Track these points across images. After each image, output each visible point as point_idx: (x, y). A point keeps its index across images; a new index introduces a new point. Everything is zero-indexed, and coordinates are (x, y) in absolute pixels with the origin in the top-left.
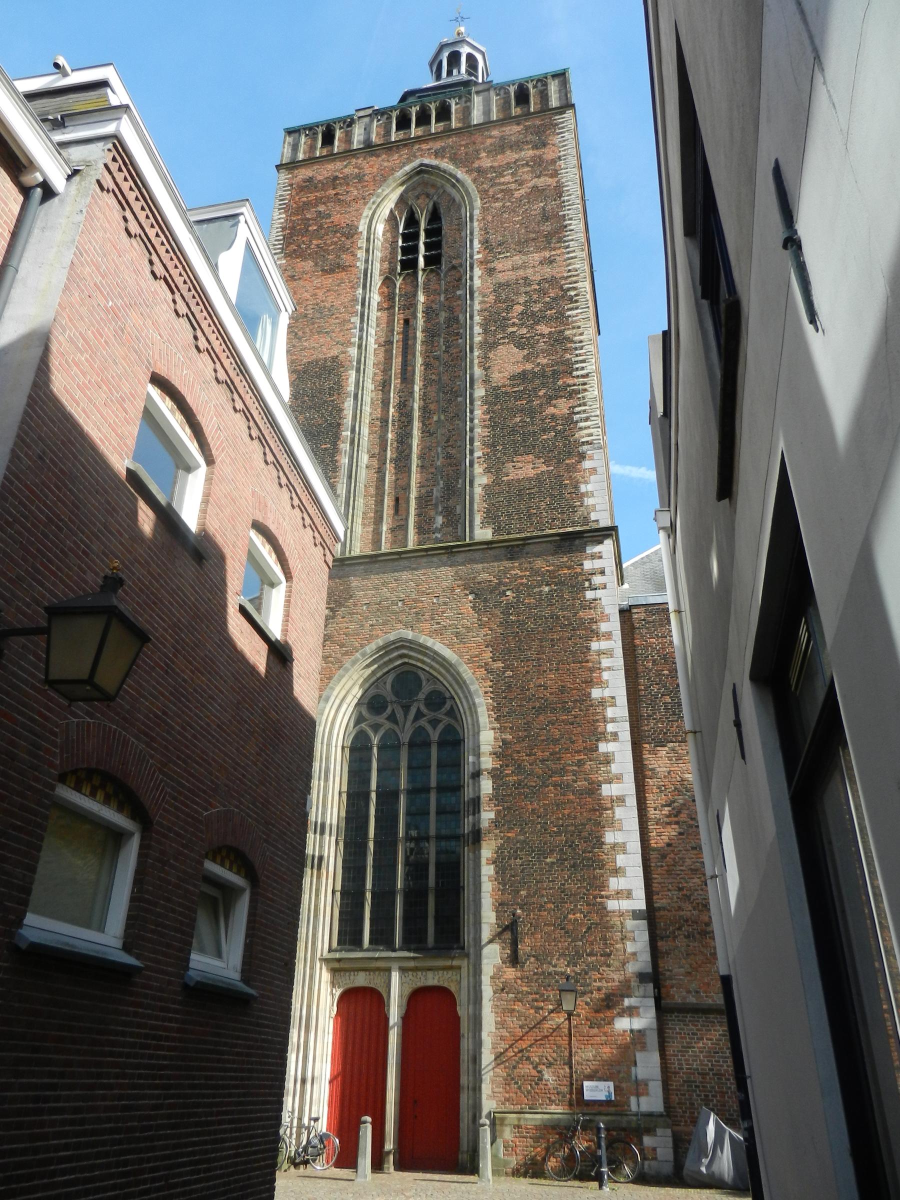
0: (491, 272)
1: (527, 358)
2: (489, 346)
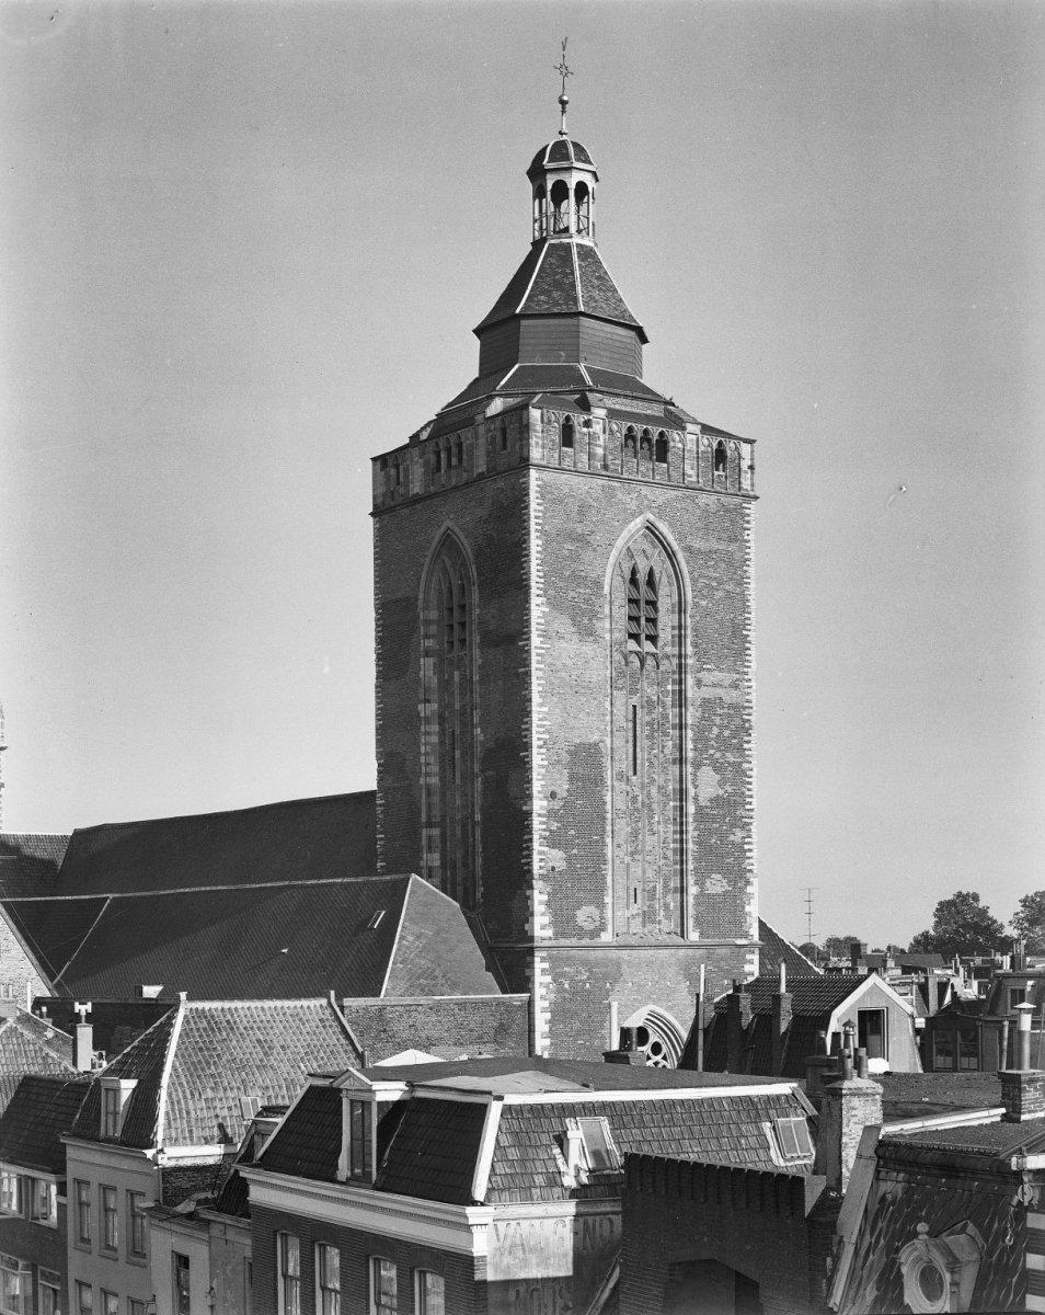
0: (699, 683)
1: (721, 784)
2: (697, 765)
